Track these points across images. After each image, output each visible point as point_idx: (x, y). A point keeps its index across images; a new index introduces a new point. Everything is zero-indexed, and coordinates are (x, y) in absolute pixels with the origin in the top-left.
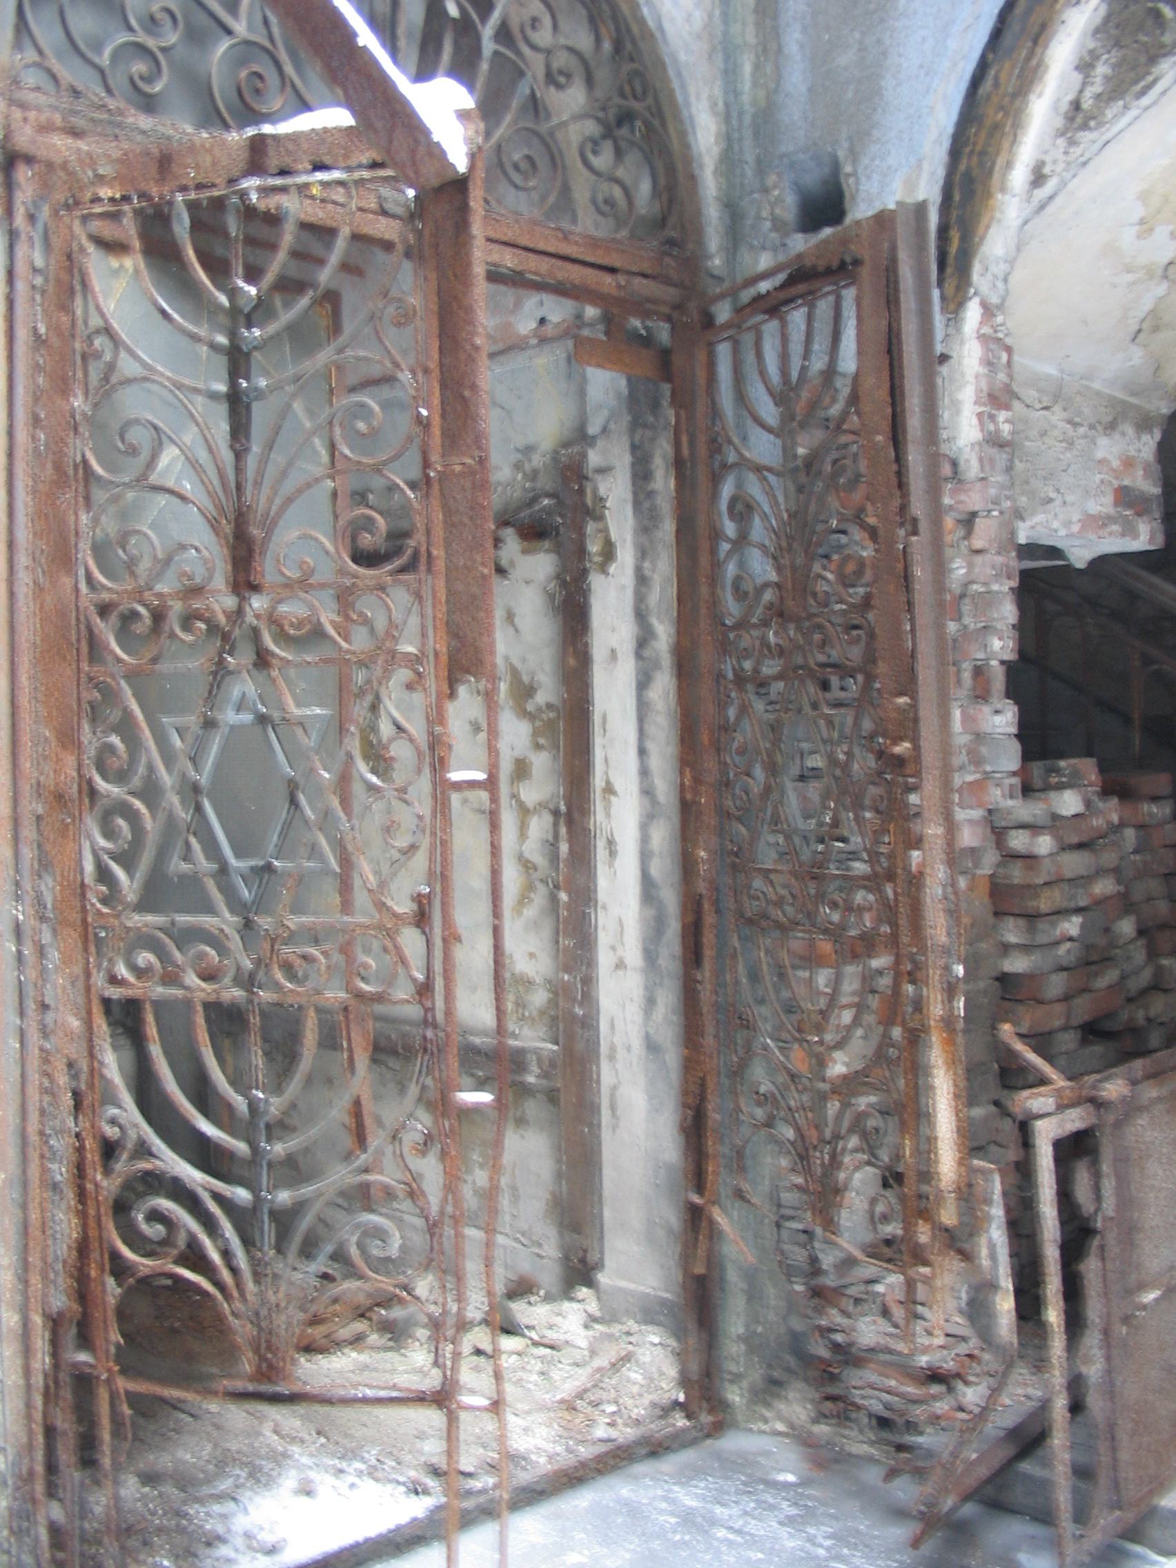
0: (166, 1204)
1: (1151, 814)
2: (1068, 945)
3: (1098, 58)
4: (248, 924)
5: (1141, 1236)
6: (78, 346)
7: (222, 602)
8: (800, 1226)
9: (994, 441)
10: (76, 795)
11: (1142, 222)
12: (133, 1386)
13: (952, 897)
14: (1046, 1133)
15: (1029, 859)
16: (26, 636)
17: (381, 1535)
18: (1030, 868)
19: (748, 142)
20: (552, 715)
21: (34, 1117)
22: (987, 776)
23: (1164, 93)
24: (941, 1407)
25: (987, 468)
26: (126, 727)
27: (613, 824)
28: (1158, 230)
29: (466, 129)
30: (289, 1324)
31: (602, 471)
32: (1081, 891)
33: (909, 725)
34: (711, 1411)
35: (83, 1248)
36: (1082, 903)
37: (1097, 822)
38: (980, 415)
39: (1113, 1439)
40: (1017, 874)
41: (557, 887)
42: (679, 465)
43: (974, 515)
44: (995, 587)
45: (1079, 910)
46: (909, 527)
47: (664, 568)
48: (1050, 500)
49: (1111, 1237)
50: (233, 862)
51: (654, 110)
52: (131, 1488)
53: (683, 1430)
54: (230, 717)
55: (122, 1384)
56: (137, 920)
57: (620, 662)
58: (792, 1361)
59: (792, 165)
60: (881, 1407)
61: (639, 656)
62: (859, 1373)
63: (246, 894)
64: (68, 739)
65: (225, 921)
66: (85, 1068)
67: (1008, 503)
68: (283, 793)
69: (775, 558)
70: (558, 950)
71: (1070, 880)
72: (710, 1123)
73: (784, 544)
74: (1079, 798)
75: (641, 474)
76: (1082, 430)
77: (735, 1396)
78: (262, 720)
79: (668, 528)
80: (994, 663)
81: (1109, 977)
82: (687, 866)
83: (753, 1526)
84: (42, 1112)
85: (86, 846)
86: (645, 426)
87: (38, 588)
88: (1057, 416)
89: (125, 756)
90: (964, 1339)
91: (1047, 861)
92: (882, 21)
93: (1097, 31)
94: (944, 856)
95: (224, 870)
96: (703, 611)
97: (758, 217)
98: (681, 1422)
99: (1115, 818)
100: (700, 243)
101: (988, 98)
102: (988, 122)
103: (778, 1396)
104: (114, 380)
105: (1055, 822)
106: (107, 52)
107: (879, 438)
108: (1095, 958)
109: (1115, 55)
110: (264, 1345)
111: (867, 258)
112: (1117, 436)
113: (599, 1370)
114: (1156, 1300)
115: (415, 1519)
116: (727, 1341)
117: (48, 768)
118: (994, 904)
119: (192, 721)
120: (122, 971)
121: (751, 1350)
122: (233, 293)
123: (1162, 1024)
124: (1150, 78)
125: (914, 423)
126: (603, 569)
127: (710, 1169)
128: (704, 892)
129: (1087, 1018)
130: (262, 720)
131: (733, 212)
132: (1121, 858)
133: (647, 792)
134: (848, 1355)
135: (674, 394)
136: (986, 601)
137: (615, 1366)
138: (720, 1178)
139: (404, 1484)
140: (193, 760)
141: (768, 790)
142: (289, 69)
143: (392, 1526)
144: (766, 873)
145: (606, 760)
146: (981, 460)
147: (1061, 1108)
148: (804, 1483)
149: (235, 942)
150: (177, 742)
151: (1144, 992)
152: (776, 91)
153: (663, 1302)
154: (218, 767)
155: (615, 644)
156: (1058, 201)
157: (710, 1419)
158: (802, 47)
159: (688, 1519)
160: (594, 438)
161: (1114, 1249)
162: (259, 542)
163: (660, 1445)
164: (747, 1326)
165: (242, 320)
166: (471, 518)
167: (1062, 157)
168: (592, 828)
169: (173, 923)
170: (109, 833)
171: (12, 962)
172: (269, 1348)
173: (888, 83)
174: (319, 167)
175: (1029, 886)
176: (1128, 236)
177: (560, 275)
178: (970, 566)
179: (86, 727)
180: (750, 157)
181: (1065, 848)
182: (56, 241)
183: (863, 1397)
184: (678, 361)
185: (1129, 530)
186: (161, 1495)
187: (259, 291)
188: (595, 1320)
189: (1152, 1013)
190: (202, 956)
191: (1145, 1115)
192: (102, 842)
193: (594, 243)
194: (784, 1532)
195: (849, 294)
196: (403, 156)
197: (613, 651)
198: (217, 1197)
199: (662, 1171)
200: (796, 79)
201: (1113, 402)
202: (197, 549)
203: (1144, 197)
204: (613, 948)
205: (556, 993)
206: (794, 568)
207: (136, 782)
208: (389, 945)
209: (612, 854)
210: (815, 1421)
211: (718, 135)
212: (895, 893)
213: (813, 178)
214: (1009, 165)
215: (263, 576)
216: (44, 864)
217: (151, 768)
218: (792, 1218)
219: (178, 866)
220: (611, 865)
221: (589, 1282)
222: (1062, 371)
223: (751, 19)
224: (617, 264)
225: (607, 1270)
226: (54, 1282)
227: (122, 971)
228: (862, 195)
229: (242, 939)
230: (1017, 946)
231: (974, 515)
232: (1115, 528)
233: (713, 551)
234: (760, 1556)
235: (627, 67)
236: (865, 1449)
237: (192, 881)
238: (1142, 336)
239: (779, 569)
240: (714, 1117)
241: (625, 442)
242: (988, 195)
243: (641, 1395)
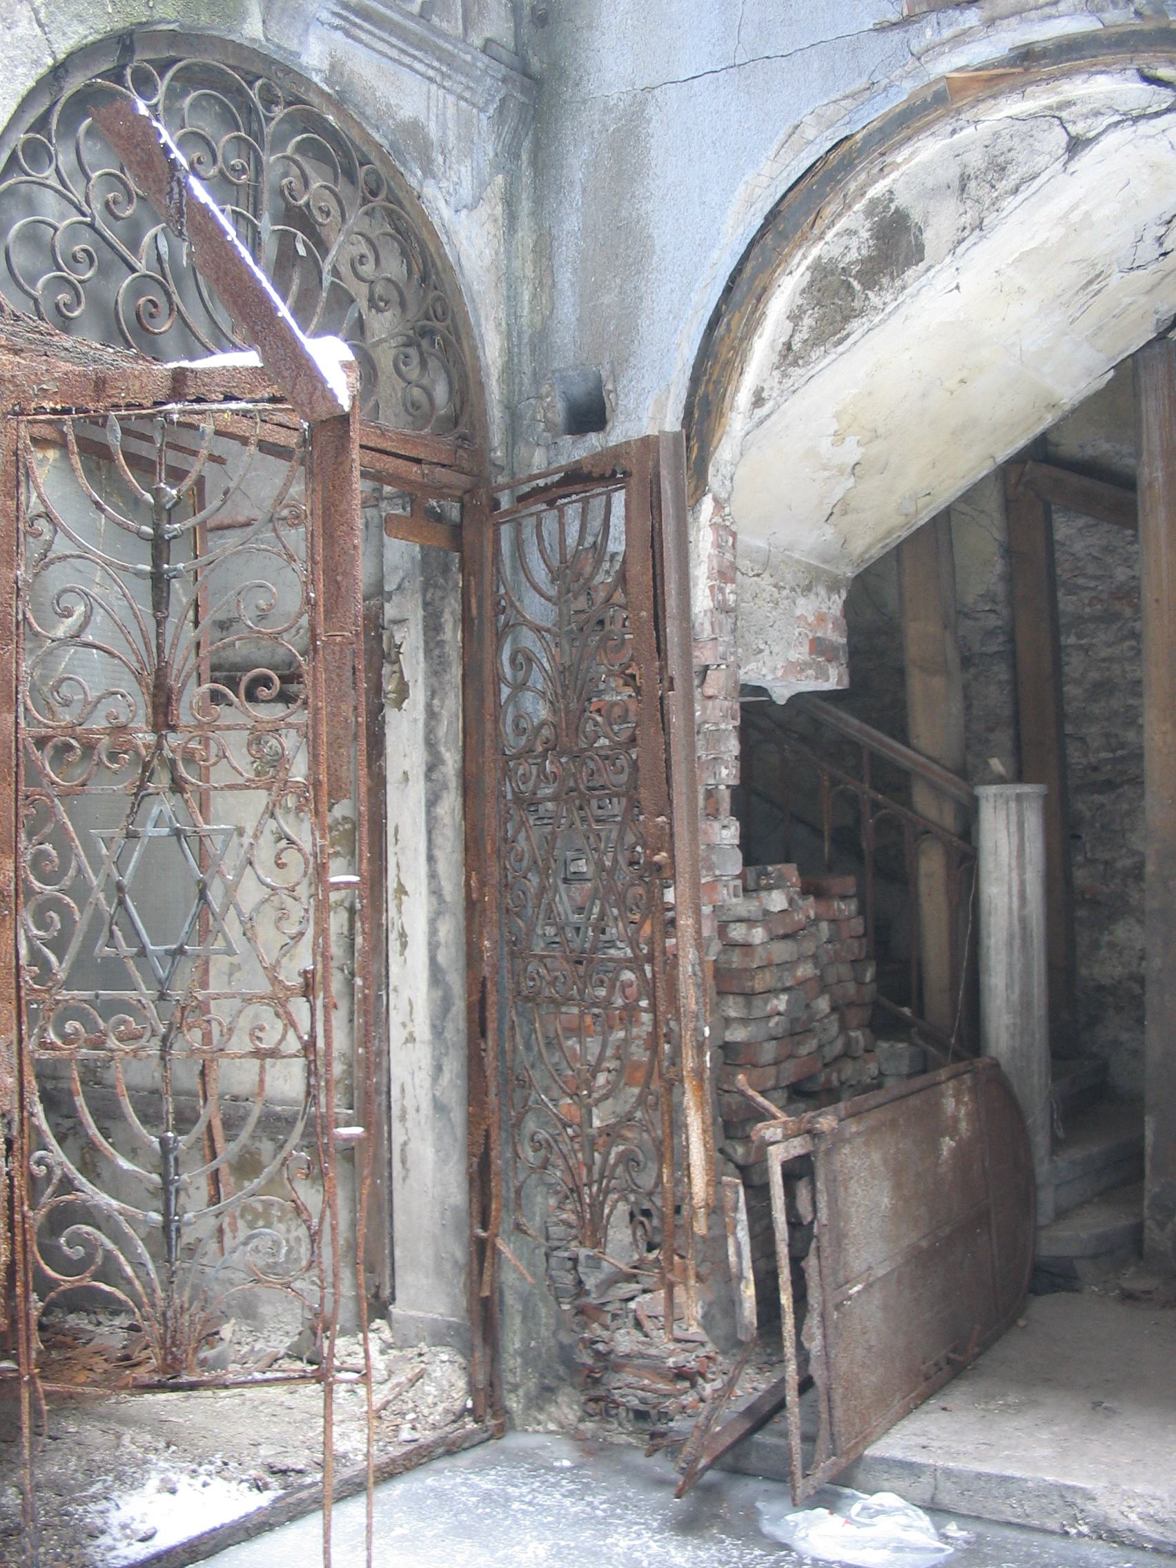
1: (840, 910)
2: (777, 1018)
3: (805, 312)
4: (162, 996)
5: (846, 1241)
7: (145, 738)
8: (566, 1254)
9: (722, 608)
11: (836, 434)
12: (49, 1387)
13: (699, 973)
14: (777, 1157)
15: (747, 946)
17: (234, 1521)
18: (746, 955)
19: (526, 358)
20: (347, 826)
22: (717, 879)
23: (855, 343)
24: (688, 1399)
25: (717, 631)
26: (61, 840)
27: (404, 919)
28: (847, 440)
29: (348, 376)
30: (192, 1322)
31: (400, 622)
32: (786, 973)
33: (667, 839)
34: (495, 1415)
35: (11, 1269)
36: (788, 984)
37: (799, 917)
38: (712, 588)
39: (829, 1400)
40: (736, 959)
41: (352, 974)
42: (466, 621)
43: (707, 668)
44: (723, 726)
45: (785, 990)
46: (666, 684)
47: (451, 705)
48: (761, 651)
49: (825, 1241)
51: (451, 329)
53: (473, 1432)
54: (150, 831)
57: (410, 783)
58: (562, 1370)
59: (563, 379)
60: (637, 1402)
61: (428, 777)
62: (618, 1376)
65: (145, 994)
66: (16, 1118)
67: (732, 658)
68: (195, 891)
69: (551, 703)
70: (352, 1028)
71: (778, 965)
72: (493, 1167)
73: (559, 691)
74: (783, 897)
75: (432, 627)
76: (785, 593)
77: (514, 1403)
79: (456, 673)
80: (722, 787)
81: (811, 1045)
82: (472, 956)
83: (540, 1498)
85: (22, 933)
86: (436, 586)
88: (766, 581)
90: (703, 1344)
91: (760, 949)
92: (639, 272)
93: (803, 291)
94: (692, 942)
95: (142, 952)
96: (488, 743)
97: (533, 418)
98: (471, 1425)
99: (812, 914)
100: (486, 438)
101: (722, 339)
102: (722, 359)
103: (549, 1401)
104: (51, 555)
105: (766, 917)
106: (40, 283)
107: (644, 613)
108: (799, 1030)
109: (818, 312)
110: (169, 1342)
111: (634, 471)
112: (812, 596)
113: (398, 1385)
114: (858, 1292)
115: (260, 1508)
116: (505, 1355)
118: (717, 984)
119: (118, 832)
120: (52, 1036)
121: (526, 1364)
122: (157, 493)
123: (851, 1086)
124: (844, 333)
125: (672, 603)
126: (398, 704)
127: (493, 1206)
128: (488, 975)
129: (792, 1079)
130: (177, 833)
131: (512, 410)
132: (817, 947)
133: (436, 892)
134: (608, 1361)
135: (462, 561)
136: (716, 738)
137: (412, 1382)
138: (503, 1219)
139: (247, 1481)
141: (543, 890)
142: (176, 298)
143: (243, 1514)
144: (542, 958)
145: (398, 866)
146: (712, 624)
147: (786, 1137)
148: (578, 1467)
149: (152, 1011)
151: (837, 1059)
152: (550, 317)
153: (450, 1326)
155: (406, 768)
156: (774, 417)
157: (494, 1422)
158: (572, 285)
159: (487, 1497)
160: (390, 594)
161: (827, 1251)
162: (175, 691)
163: (454, 1443)
164: (522, 1342)
165: (165, 516)
166: (338, 675)
167: (776, 386)
168: (384, 922)
169: (97, 996)
170: (42, 924)
172: (174, 1344)
173: (643, 322)
174: (229, 398)
175: (745, 970)
176: (825, 444)
177: (379, 466)
178: (704, 709)
180: (527, 369)
181: (773, 938)
183: (622, 1396)
184: (468, 535)
185: (822, 674)
187: (179, 491)
188: (390, 1346)
189: (843, 1078)
191: (847, 1146)
193: (405, 440)
194: (567, 1502)
195: (619, 499)
196: (303, 397)
197: (405, 773)
199: (448, 1213)
200: (568, 310)
201: (809, 568)
202: (123, 696)
203: (837, 416)
204: (404, 1025)
205: (350, 1066)
206: (567, 712)
207: (67, 882)
208: (281, 1011)
209: (404, 945)
210: (581, 1420)
211: (501, 350)
212: (653, 971)
213: (579, 389)
214: (737, 390)
217: (80, 870)
218: (558, 1248)
219: (103, 950)
220: (402, 954)
221: (383, 1313)
222: (770, 545)
223: (530, 257)
224: (422, 456)
225: (397, 1302)
227: (52, 1036)
228: (621, 408)
230: (736, 1019)
231: (707, 668)
232: (811, 672)
233: (497, 693)
234: (550, 1519)
235: (432, 294)
236: (623, 1439)
238: (833, 517)
239: (555, 711)
240: (497, 1163)
241: (418, 598)
242: (722, 415)
243: (435, 1404)
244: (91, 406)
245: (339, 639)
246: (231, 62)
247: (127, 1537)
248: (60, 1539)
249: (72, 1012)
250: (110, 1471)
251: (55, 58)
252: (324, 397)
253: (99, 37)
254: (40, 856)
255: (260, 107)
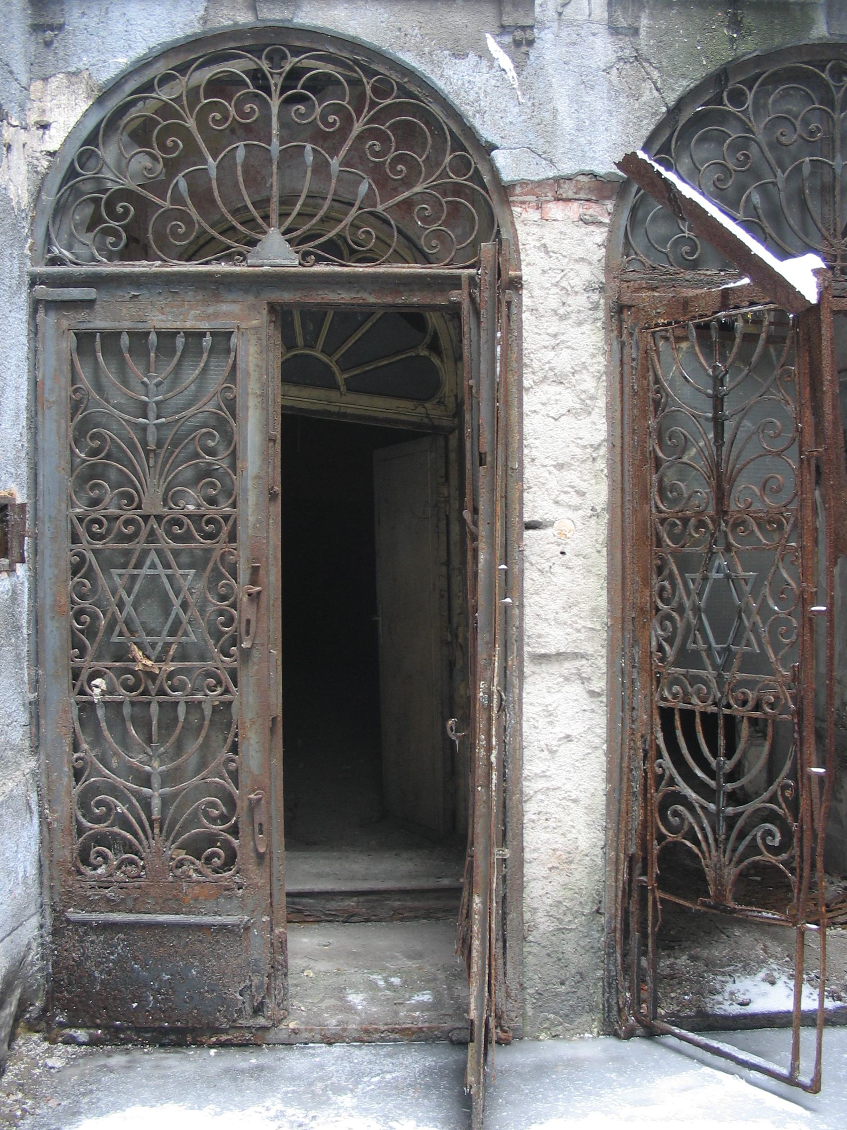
0: (680, 808)
6: (650, 394)
10: (649, 609)
12: (663, 896)
16: (629, 533)
21: (626, 759)
26: (671, 578)
30: (729, 874)
35: (645, 824)
50: (714, 644)
52: (683, 960)
54: (714, 575)
55: (659, 894)
56: (673, 670)
63: (719, 661)
64: (646, 582)
65: (709, 673)
78: (728, 577)
84: (630, 758)
87: (635, 511)
89: (670, 591)
117: (638, 595)
119: (698, 576)
130: (728, 577)
140: (698, 594)
149: (714, 685)
150: (692, 586)
154: (708, 599)
170: (664, 629)
171: (620, 686)
174: (752, 304)
179: (654, 577)
182: (641, 345)
186: (695, 965)
190: (700, 689)
192: (660, 632)
198: (703, 808)
207: (674, 604)
215: (729, 506)
216: (635, 642)
217: (681, 598)
219: (691, 646)
226: (631, 839)
227: (666, 694)
229: (717, 682)
237: (696, 653)
244: (681, 319)
245: (815, 453)
246: (805, 59)
247: (732, 1000)
248: (691, 988)
249: (676, 681)
250: (742, 961)
251: (667, 107)
252: (796, 298)
253: (697, 82)
254: (662, 589)
255: (831, 82)
